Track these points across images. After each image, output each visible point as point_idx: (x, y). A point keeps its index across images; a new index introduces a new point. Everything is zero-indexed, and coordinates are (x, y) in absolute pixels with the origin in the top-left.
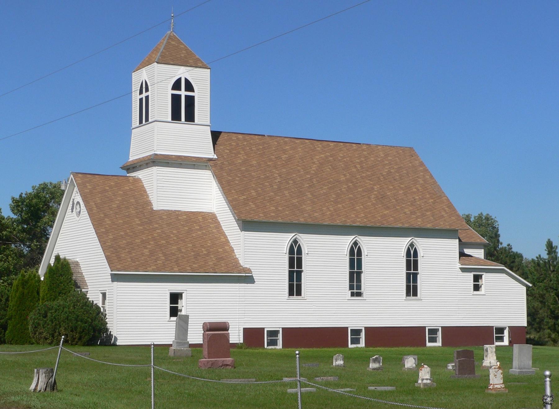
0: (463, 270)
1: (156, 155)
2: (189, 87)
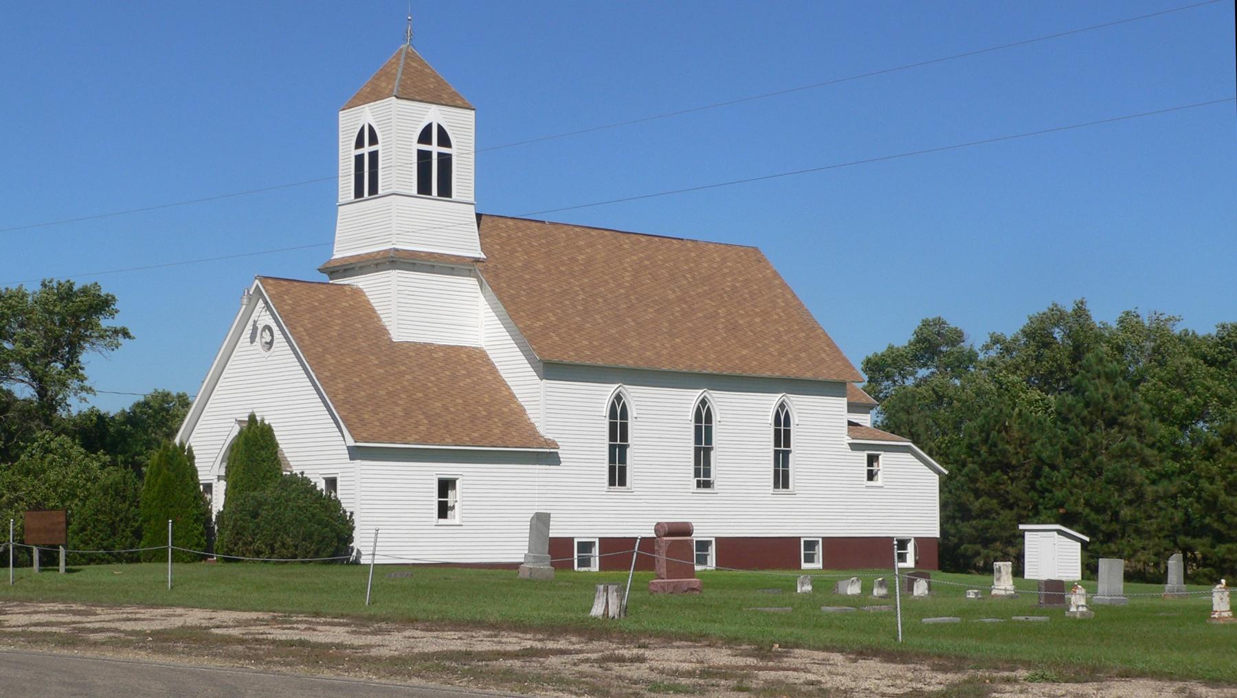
0: (854, 447)
1: (397, 250)
2: (444, 140)
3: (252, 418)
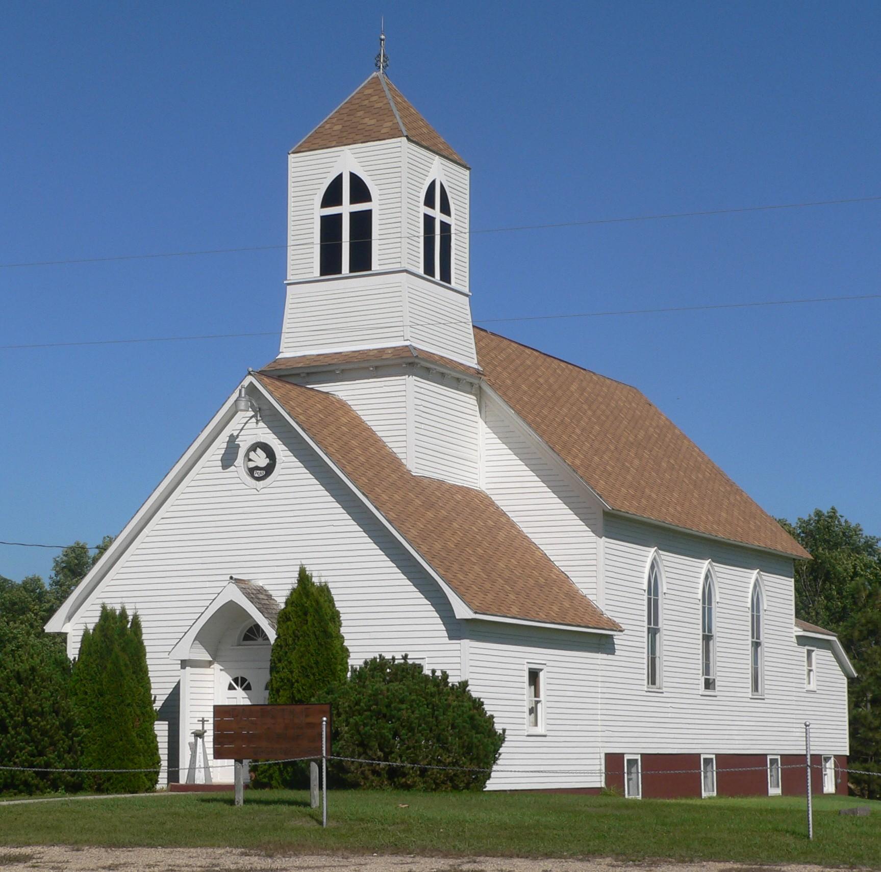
2: (360, 191)
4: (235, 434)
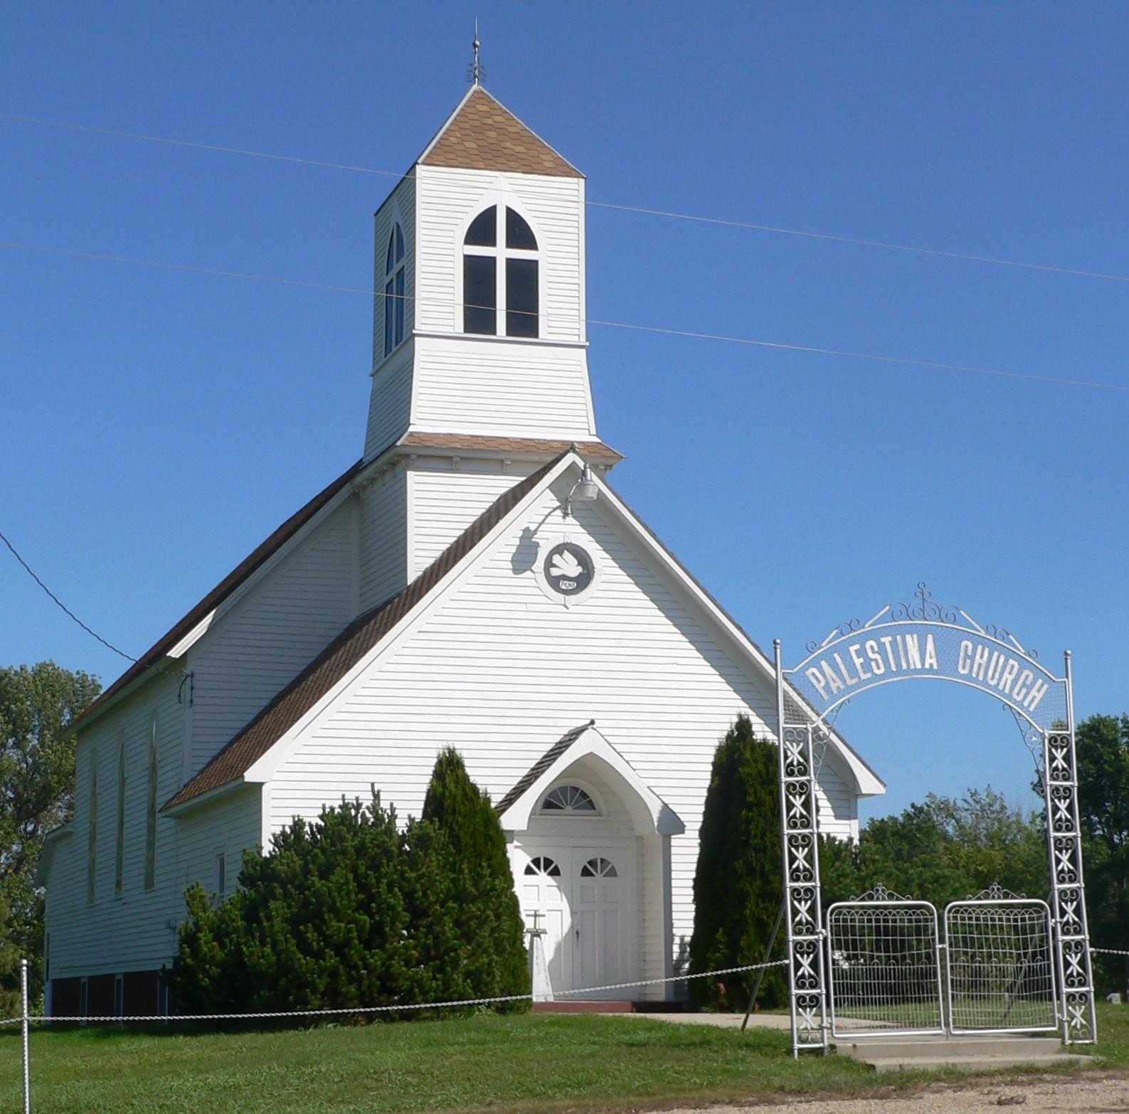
2: (520, 234)
3: (872, 819)
4: (533, 527)
